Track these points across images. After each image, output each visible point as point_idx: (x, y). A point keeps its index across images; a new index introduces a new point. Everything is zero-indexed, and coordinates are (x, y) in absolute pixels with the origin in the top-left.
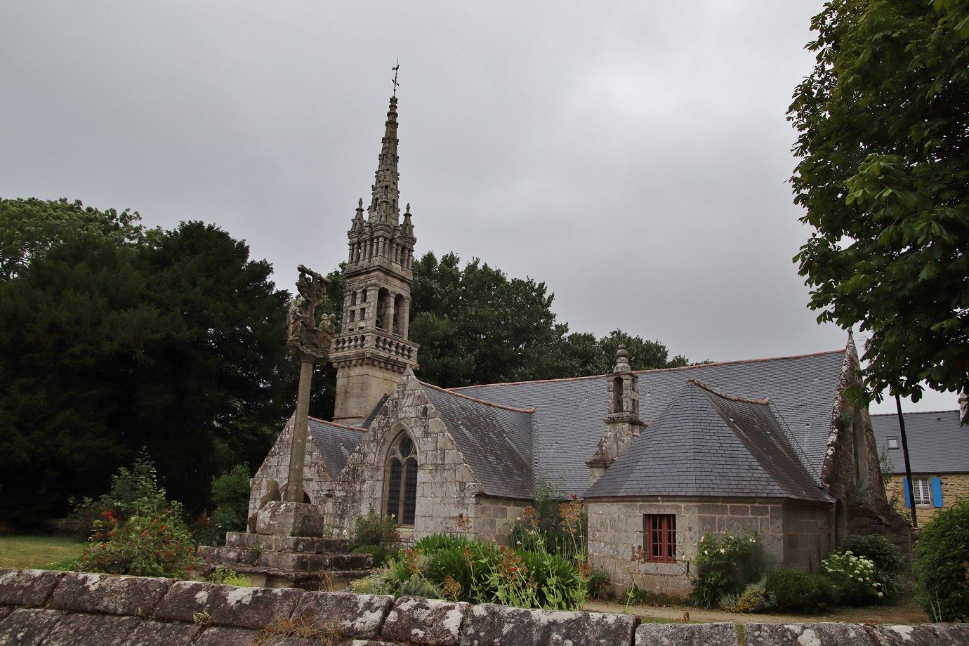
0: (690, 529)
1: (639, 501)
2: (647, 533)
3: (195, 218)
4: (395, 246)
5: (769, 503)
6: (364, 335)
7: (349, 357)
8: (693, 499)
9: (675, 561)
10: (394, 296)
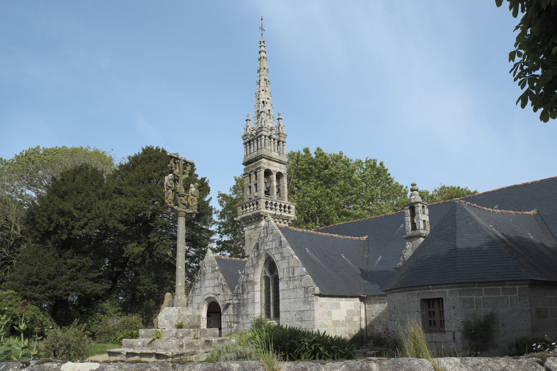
0: (454, 308)
1: (416, 290)
2: (425, 312)
4: (272, 140)
5: (517, 285)
8: (455, 286)
9: (445, 332)
10: (276, 173)
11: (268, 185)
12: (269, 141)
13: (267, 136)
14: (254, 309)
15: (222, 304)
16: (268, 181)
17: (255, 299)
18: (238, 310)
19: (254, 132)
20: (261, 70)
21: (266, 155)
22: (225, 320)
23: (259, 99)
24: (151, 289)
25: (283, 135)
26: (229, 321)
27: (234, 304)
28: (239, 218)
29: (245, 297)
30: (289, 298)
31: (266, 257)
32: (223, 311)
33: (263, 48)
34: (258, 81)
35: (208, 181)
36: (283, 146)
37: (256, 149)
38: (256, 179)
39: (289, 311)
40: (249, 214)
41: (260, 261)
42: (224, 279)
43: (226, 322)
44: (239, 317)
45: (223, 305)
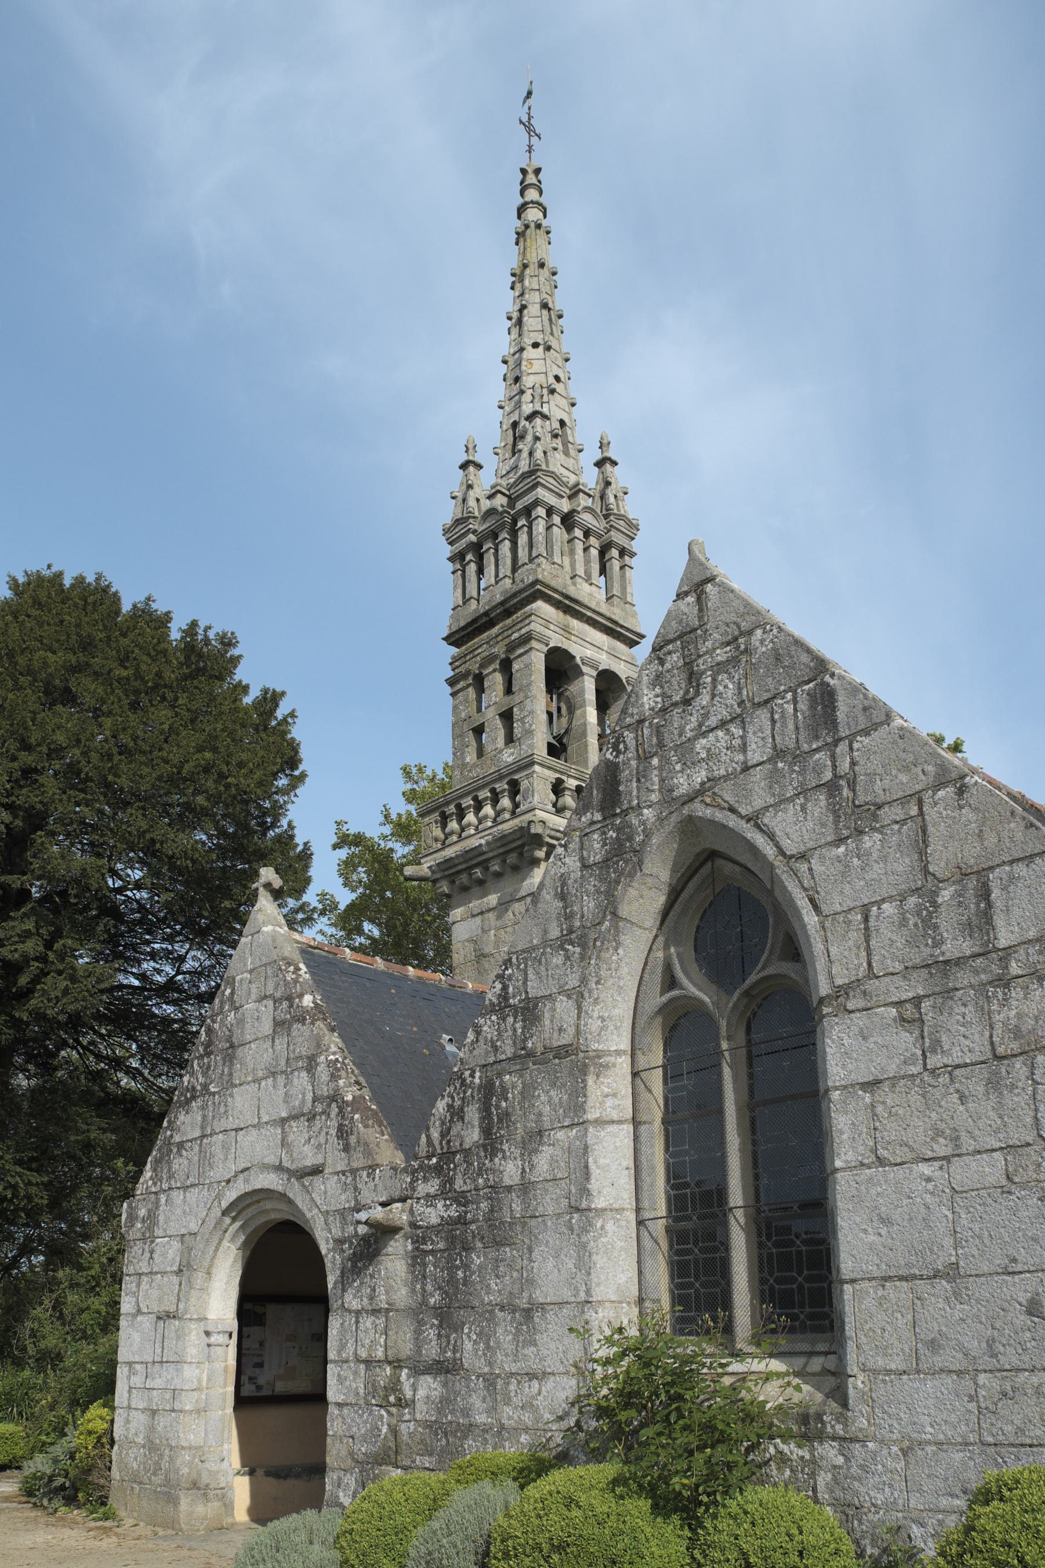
3: (37, 565)
4: (578, 533)
6: (516, 777)
7: (476, 851)
10: (595, 673)
11: (559, 724)
12: (566, 537)
13: (559, 512)
14: (584, 1264)
15: (337, 1232)
16: (559, 709)
17: (594, 1185)
18: (452, 1269)
19: (500, 501)
20: (528, 271)
21: (553, 583)
22: (350, 1348)
23: (517, 379)
24: (14, 1187)
25: (622, 522)
26: (380, 1353)
27: (419, 1234)
28: (425, 866)
29: (510, 1171)
30: (942, 1148)
31: (679, 853)
32: (344, 1282)
33: (532, 195)
34: (515, 315)
35: (292, 714)
36: (622, 568)
37: (506, 569)
38: (509, 691)
39: (952, 1273)
40: (474, 842)
41: (632, 892)
42: (351, 1066)
43: (358, 1360)
44: (458, 1328)
45: (339, 1242)
